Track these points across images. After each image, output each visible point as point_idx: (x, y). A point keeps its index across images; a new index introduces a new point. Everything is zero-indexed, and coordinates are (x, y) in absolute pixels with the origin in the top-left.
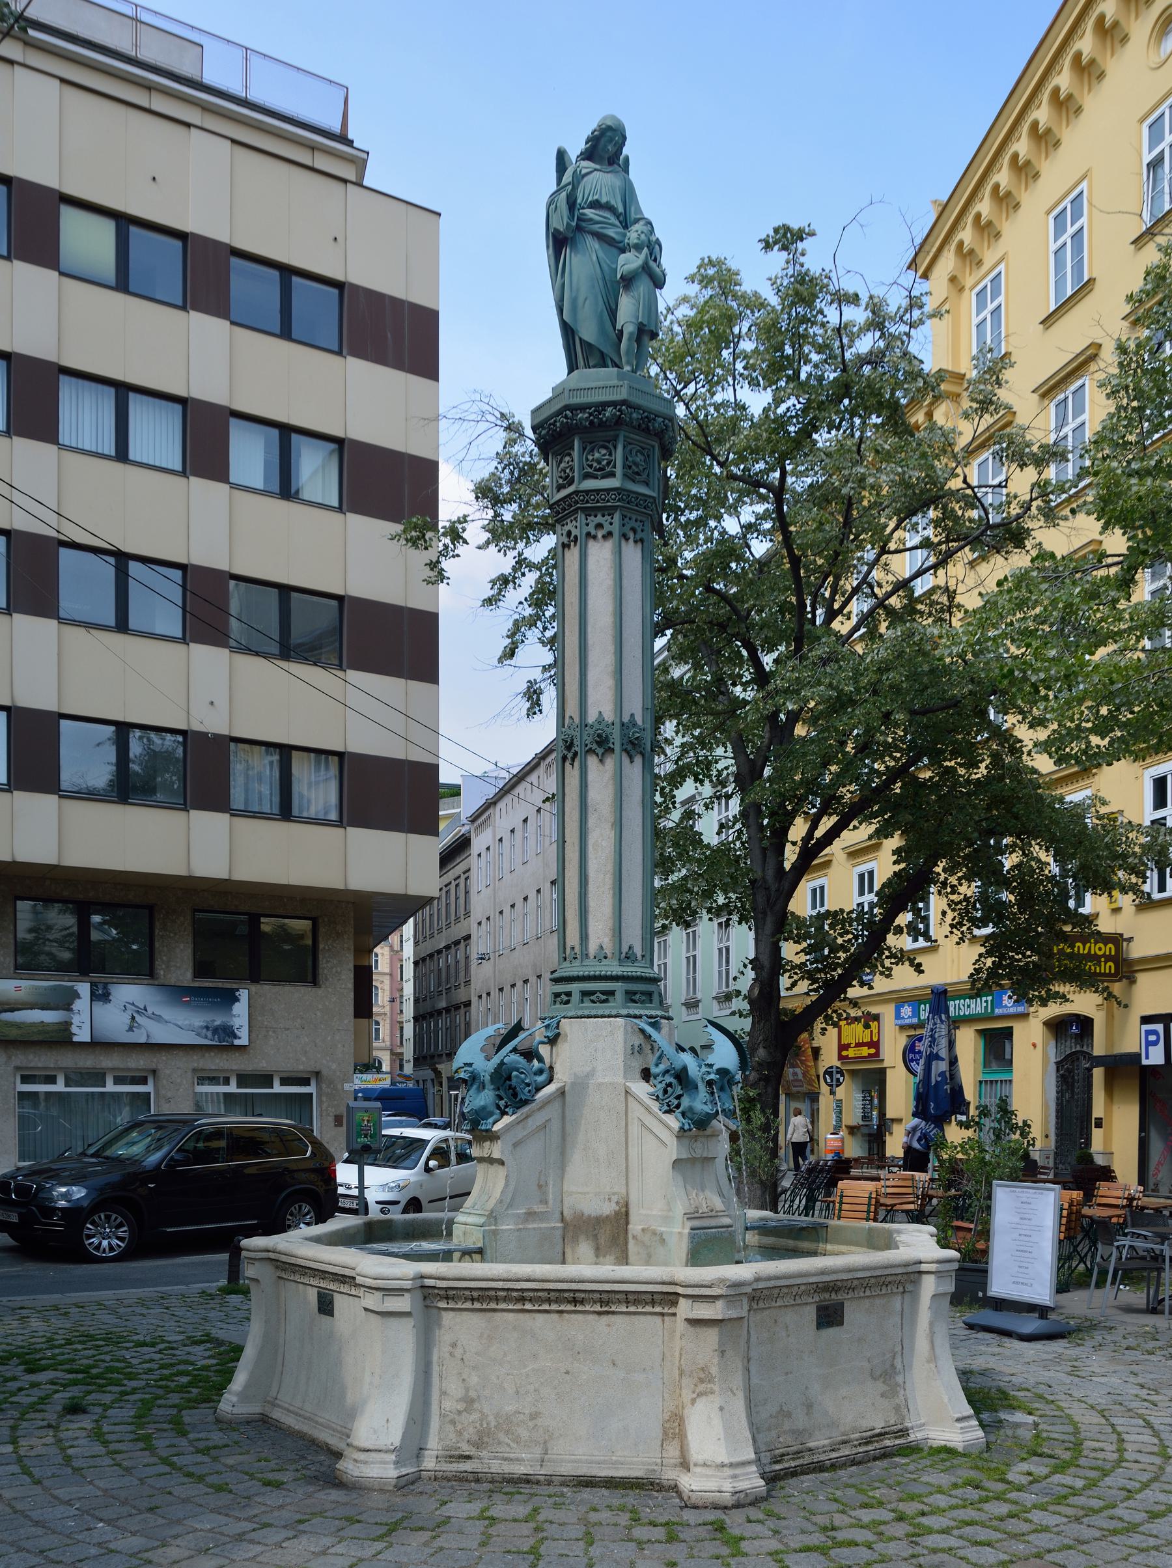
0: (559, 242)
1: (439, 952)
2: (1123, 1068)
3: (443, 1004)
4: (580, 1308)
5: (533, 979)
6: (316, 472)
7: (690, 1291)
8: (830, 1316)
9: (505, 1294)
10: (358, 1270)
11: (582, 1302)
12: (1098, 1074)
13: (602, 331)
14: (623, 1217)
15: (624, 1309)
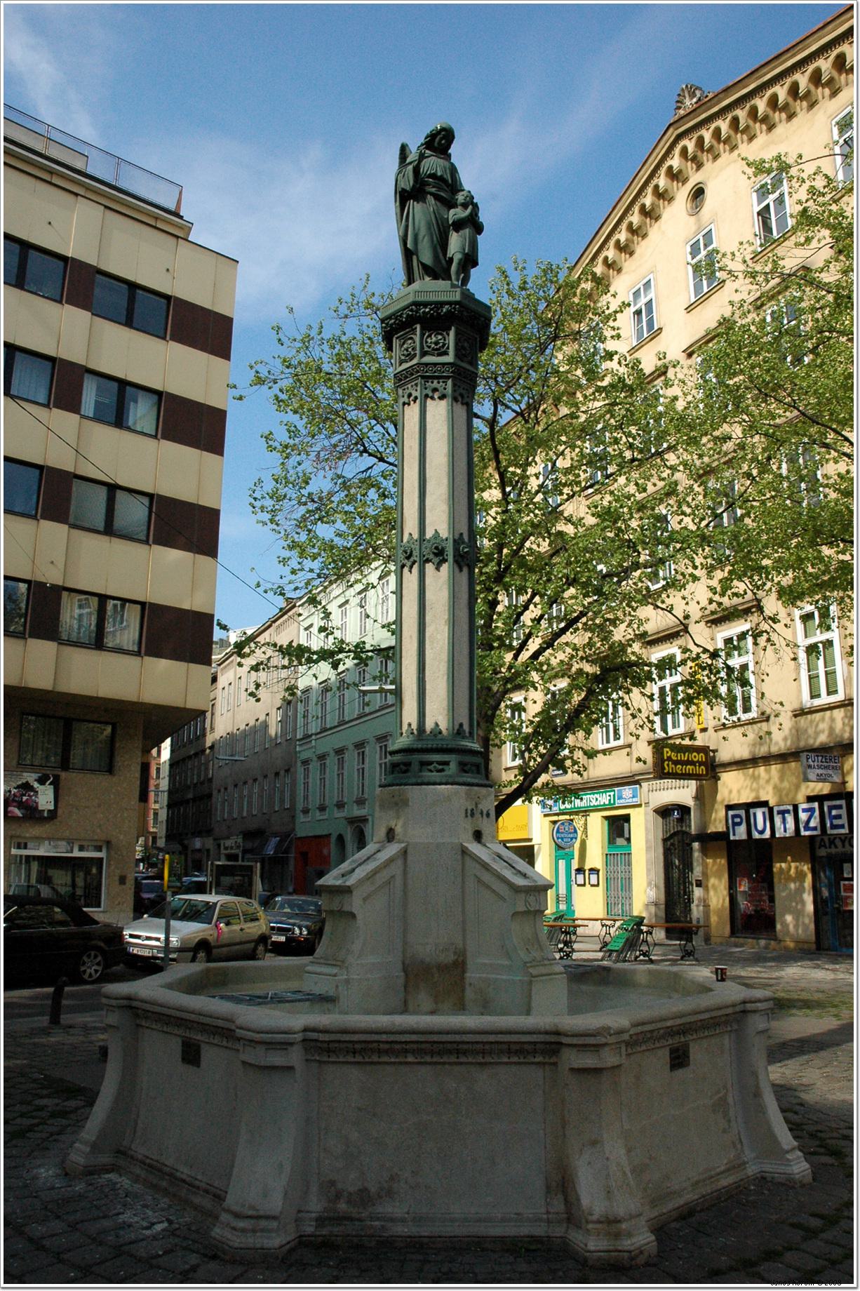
0: (404, 197)
1: (190, 757)
2: (711, 841)
3: (190, 796)
4: (463, 1059)
5: (260, 779)
6: (142, 413)
7: (575, 1041)
8: (679, 1059)
9: (363, 1046)
10: (238, 1022)
11: (465, 1053)
12: (696, 845)
13: (436, 257)
14: (458, 966)
15: (506, 1060)
